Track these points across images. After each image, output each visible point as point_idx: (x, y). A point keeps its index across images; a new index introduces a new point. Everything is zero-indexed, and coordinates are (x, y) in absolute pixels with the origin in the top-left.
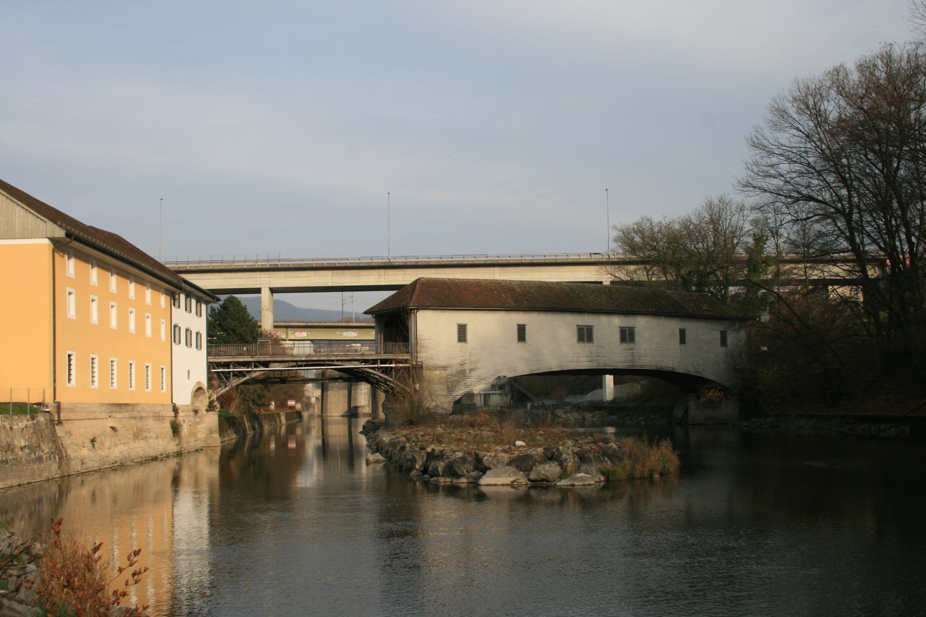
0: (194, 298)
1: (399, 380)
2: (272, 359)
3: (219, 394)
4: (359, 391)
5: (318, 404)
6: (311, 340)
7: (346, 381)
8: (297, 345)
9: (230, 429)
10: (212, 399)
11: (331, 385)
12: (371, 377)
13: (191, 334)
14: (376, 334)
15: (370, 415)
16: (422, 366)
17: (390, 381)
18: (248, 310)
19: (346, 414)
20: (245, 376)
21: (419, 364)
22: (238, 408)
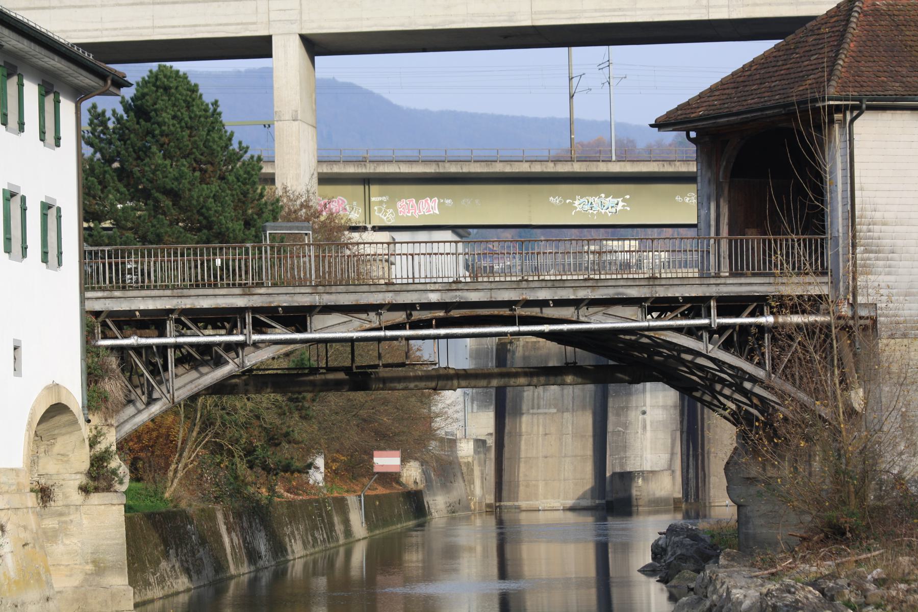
0: (32, 79)
1: (788, 376)
2: (316, 300)
3: (128, 428)
4: (634, 415)
5: (483, 464)
6: (453, 228)
7: (594, 382)
8: (405, 249)
9: (166, 556)
10: (100, 447)
11: (529, 393)
12: (684, 362)
13: (24, 210)
14: (699, 204)
15: (676, 505)
16: (875, 321)
17: (753, 379)
18: (224, 118)
19: (587, 503)
20: (219, 362)
21: (863, 313)
22: (193, 479)
